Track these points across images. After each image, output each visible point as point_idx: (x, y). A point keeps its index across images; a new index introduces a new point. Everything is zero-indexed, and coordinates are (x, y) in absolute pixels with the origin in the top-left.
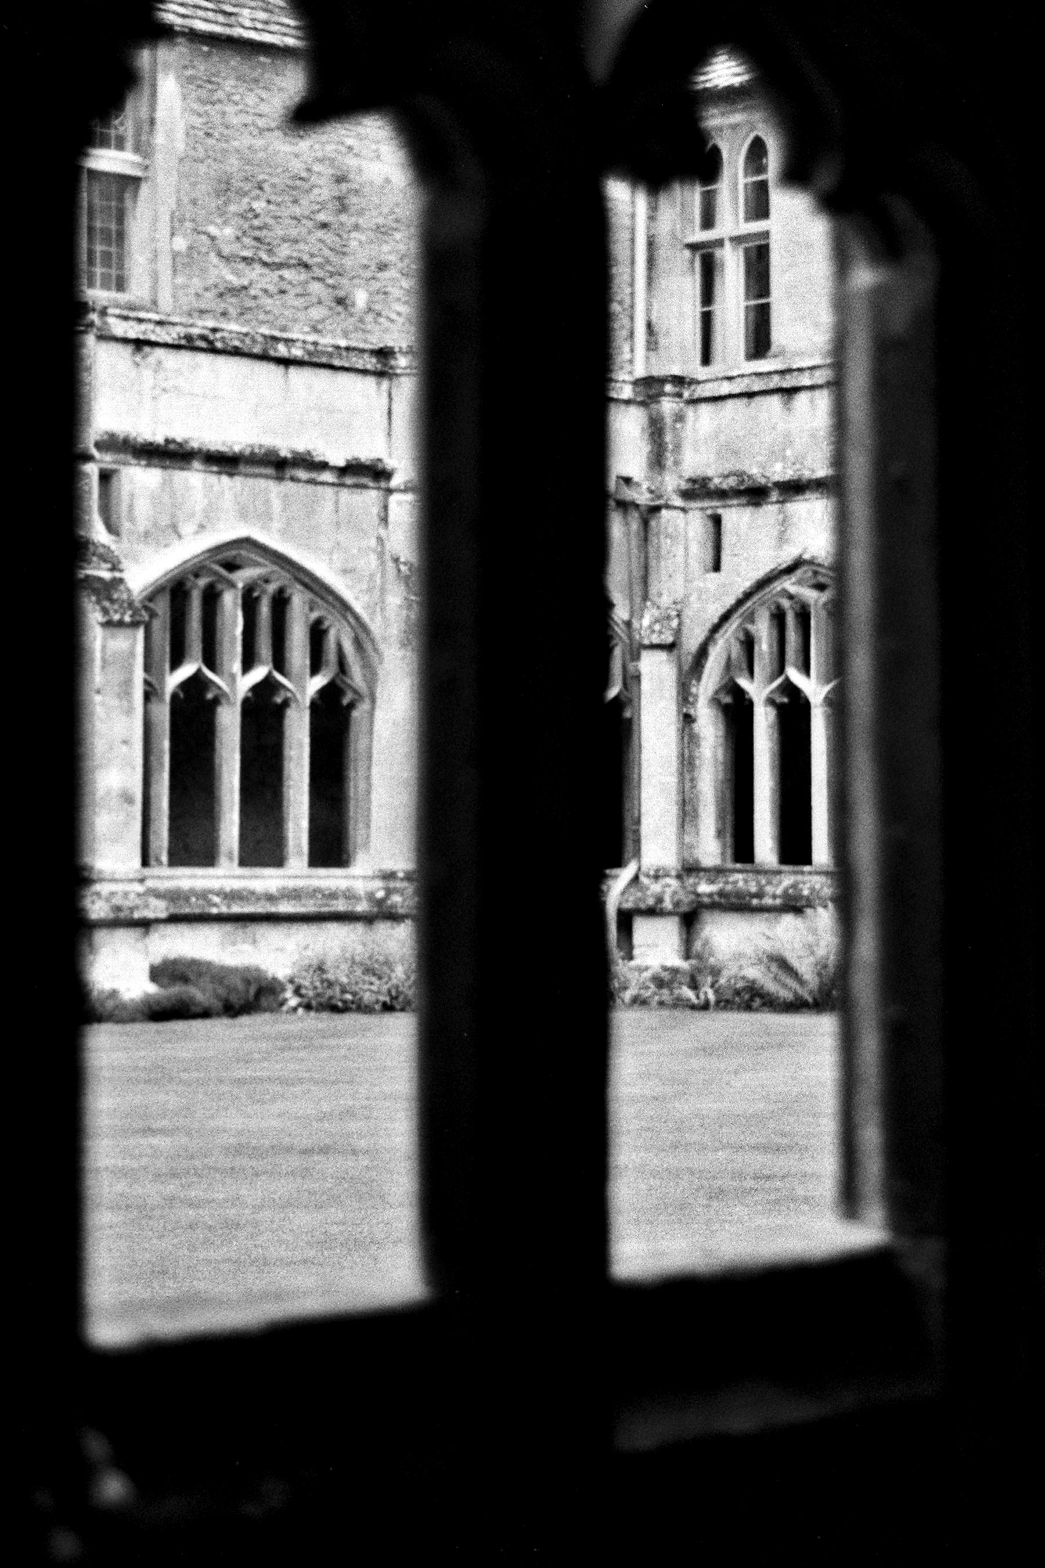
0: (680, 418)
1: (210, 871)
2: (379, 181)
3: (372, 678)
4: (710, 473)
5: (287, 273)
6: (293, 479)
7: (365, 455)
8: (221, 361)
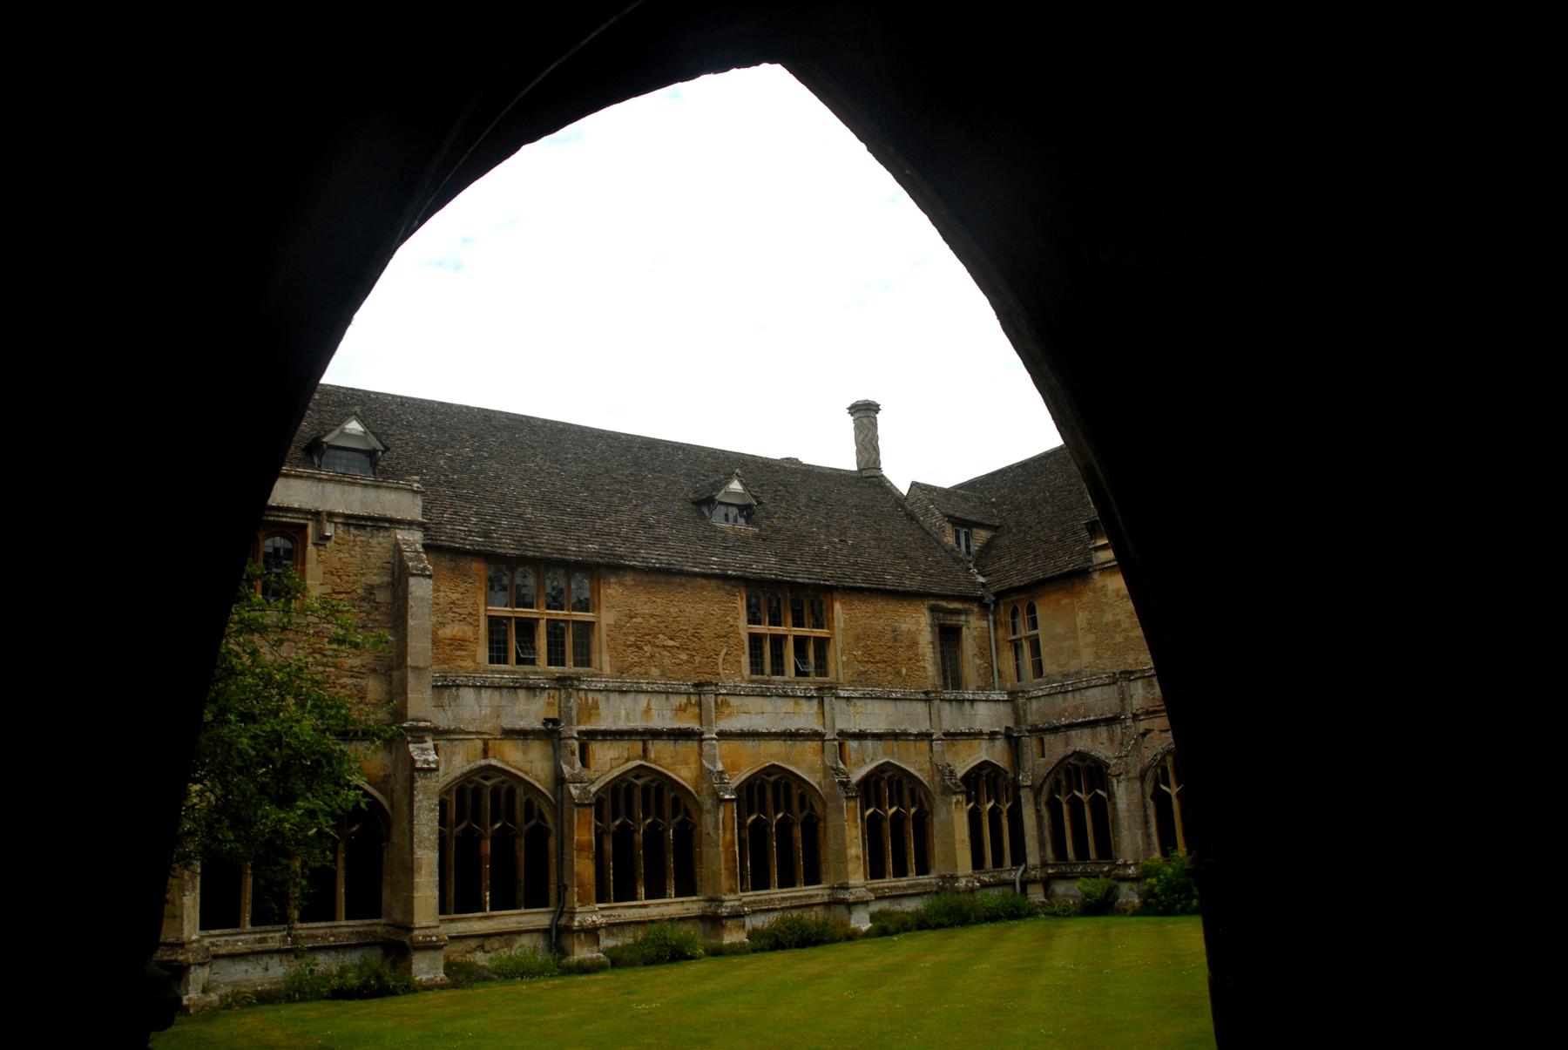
0: (1025, 704)
2: (907, 629)
3: (931, 806)
4: (1038, 723)
5: (879, 665)
6: (901, 740)
7: (924, 730)
8: (875, 701)
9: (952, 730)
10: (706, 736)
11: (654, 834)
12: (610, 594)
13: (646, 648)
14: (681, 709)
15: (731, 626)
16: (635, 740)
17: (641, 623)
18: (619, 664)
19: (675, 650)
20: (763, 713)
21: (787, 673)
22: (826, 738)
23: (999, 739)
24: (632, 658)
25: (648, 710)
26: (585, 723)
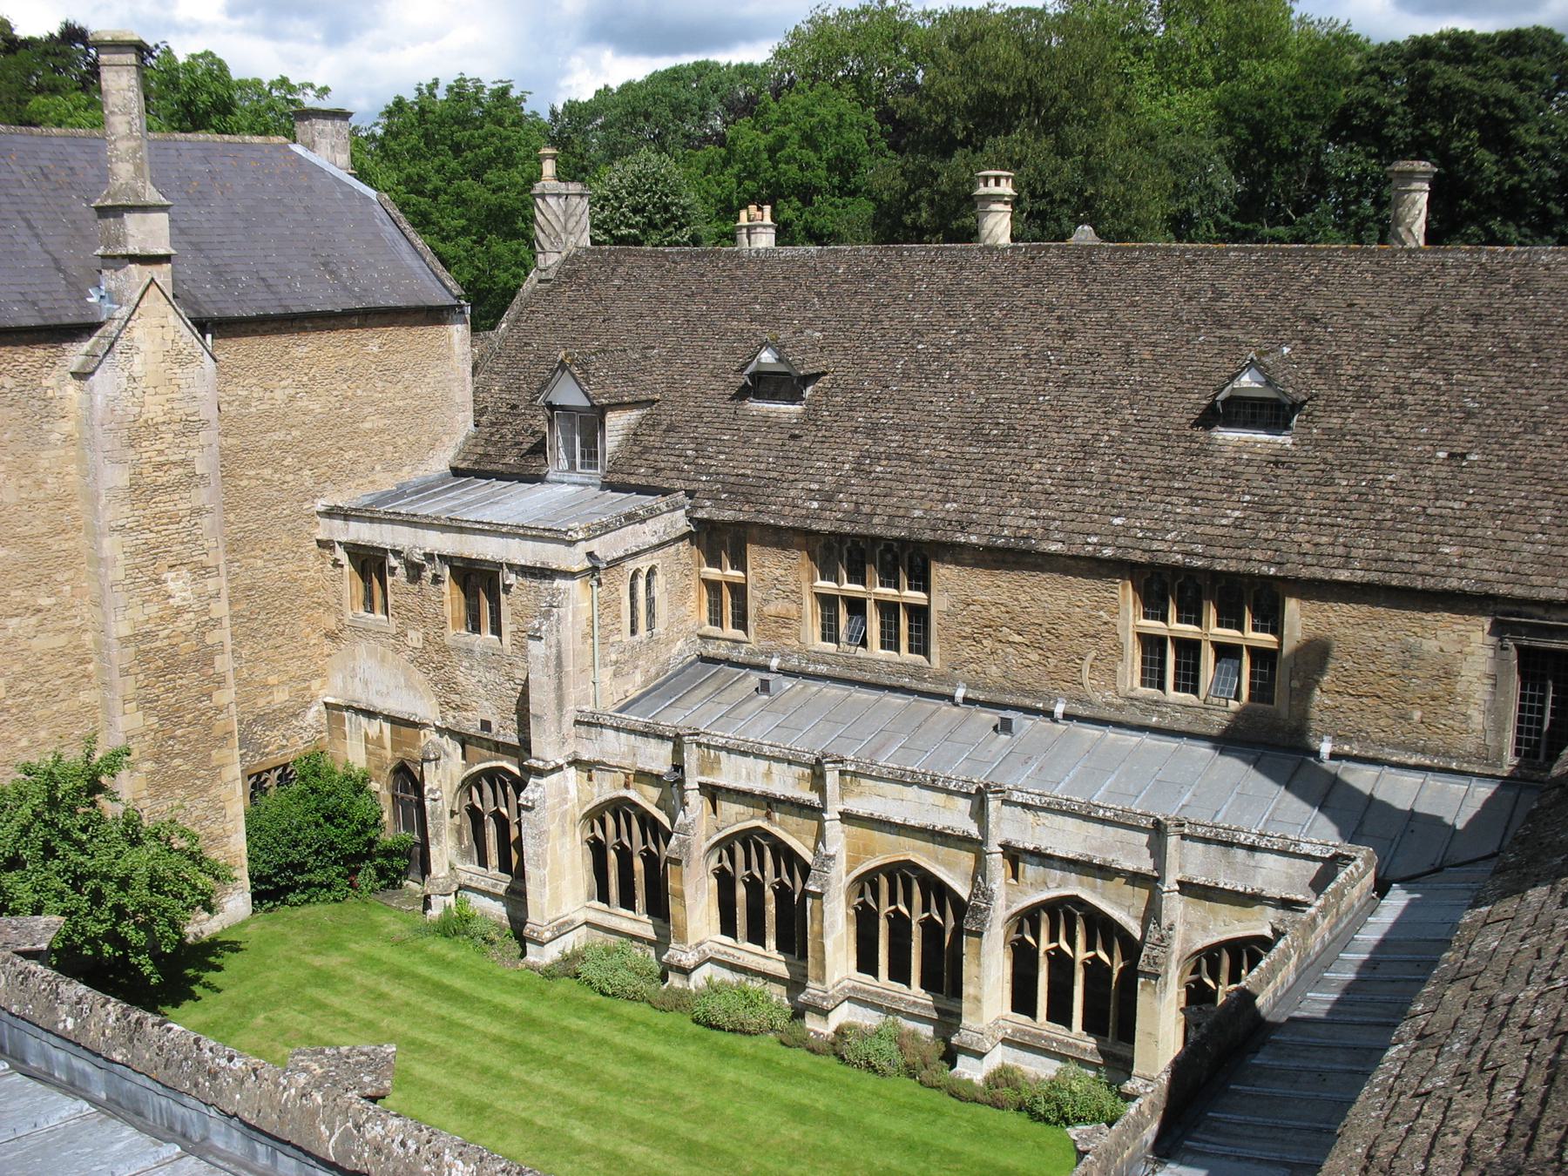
5: (1364, 700)
9: (1201, 880)
15: (1105, 623)
18: (952, 658)
19: (1025, 648)
25: (768, 774)
26: (708, 775)
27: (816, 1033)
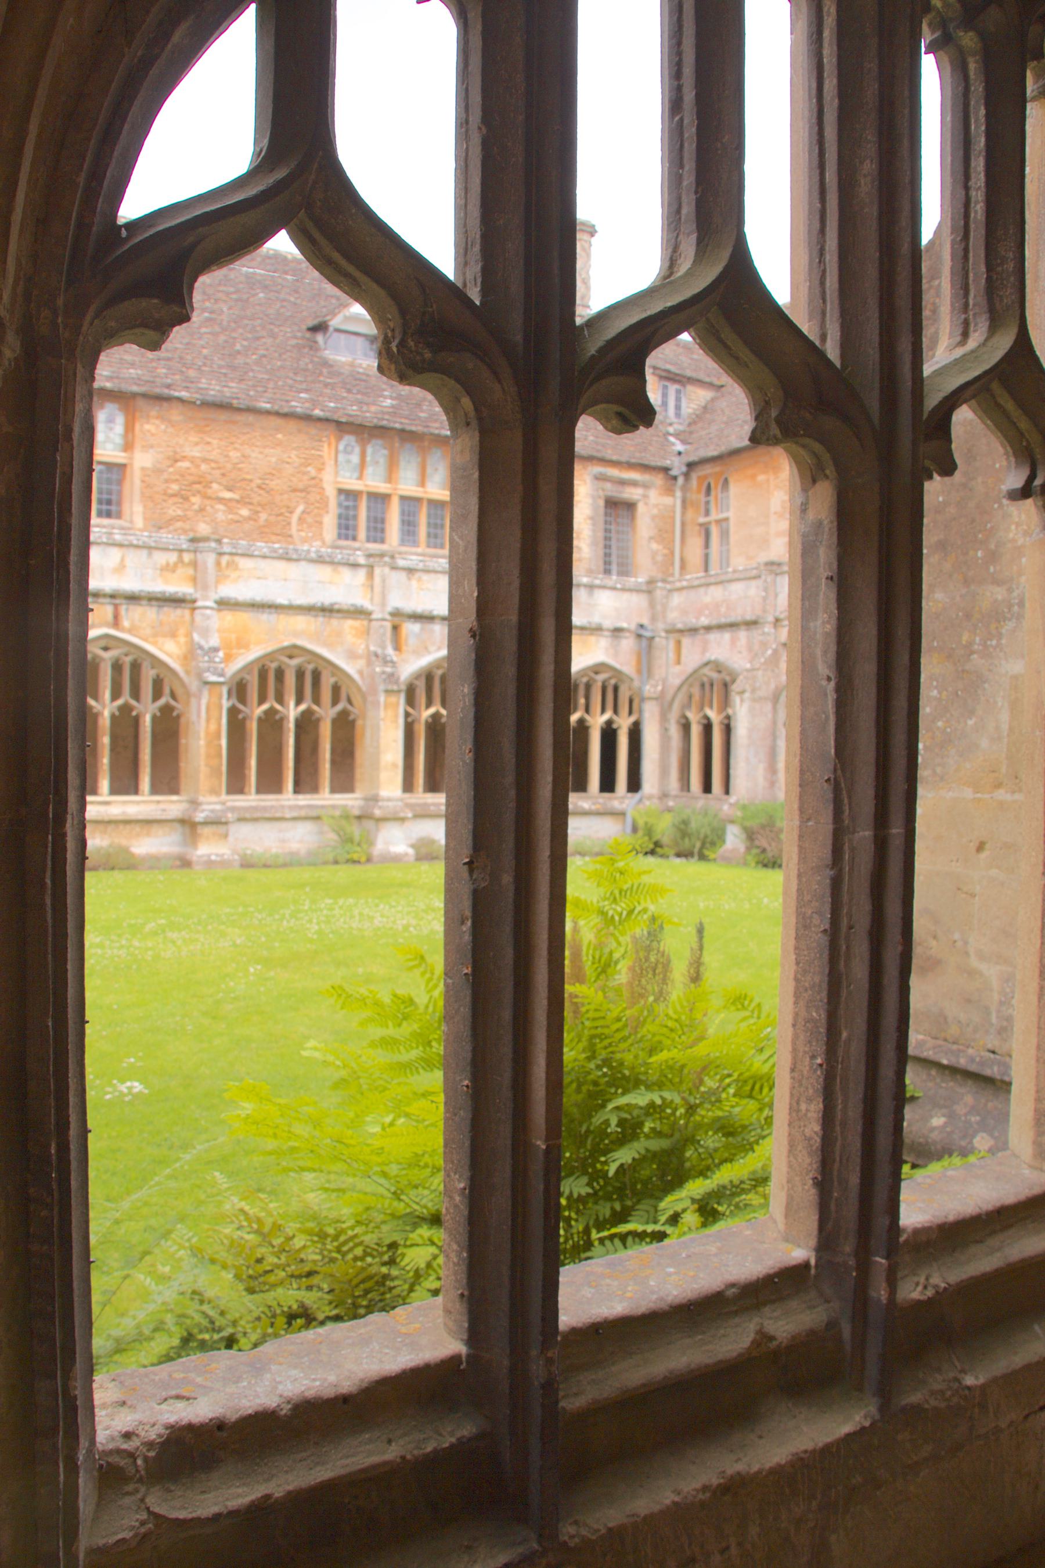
1: (316, 796)
10: (199, 604)
11: (306, 725)
12: (149, 431)
13: (193, 499)
14: (168, 569)
15: (313, 478)
16: (102, 604)
17: (188, 468)
19: (234, 504)
20: (285, 580)
21: (388, 540)
22: (374, 616)
23: (626, 638)
24: (173, 511)
25: (120, 569)
27: (217, 855)
